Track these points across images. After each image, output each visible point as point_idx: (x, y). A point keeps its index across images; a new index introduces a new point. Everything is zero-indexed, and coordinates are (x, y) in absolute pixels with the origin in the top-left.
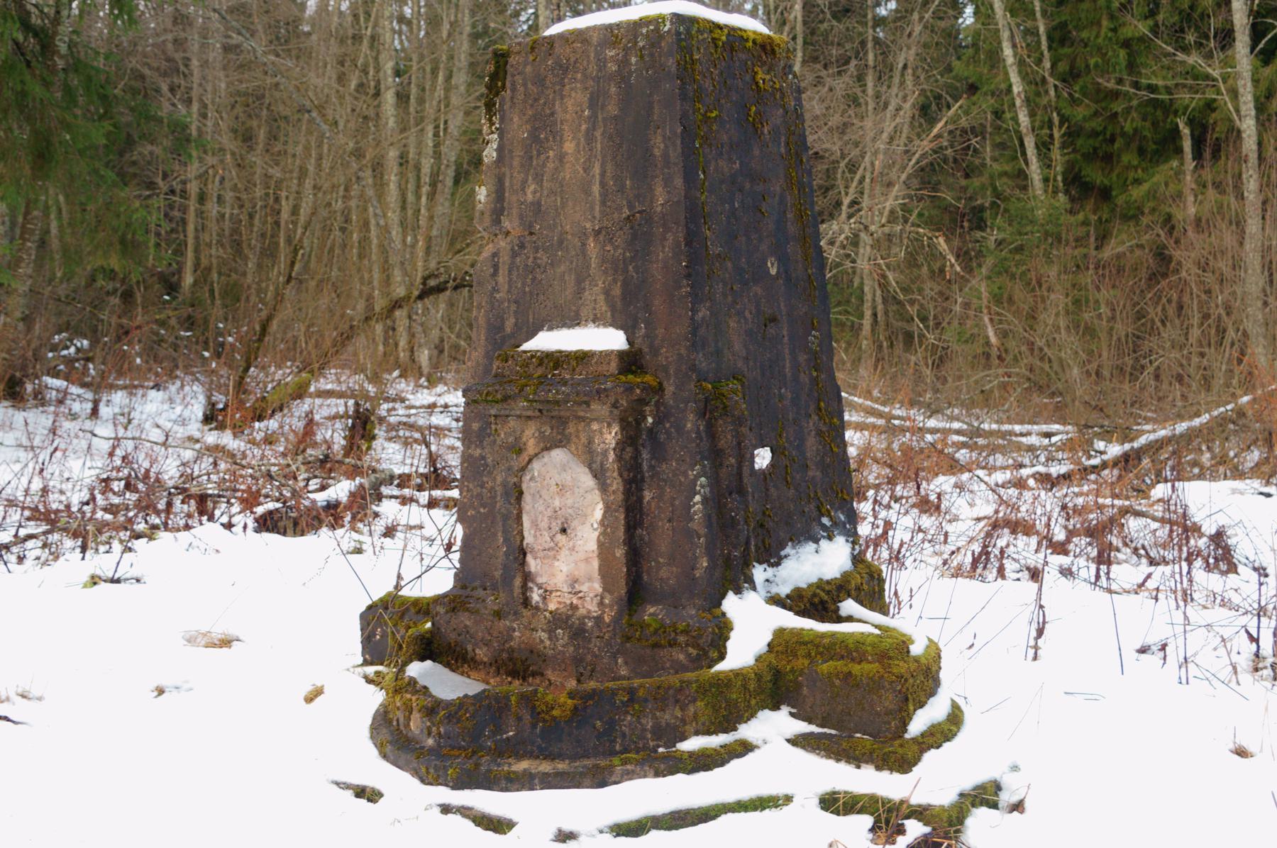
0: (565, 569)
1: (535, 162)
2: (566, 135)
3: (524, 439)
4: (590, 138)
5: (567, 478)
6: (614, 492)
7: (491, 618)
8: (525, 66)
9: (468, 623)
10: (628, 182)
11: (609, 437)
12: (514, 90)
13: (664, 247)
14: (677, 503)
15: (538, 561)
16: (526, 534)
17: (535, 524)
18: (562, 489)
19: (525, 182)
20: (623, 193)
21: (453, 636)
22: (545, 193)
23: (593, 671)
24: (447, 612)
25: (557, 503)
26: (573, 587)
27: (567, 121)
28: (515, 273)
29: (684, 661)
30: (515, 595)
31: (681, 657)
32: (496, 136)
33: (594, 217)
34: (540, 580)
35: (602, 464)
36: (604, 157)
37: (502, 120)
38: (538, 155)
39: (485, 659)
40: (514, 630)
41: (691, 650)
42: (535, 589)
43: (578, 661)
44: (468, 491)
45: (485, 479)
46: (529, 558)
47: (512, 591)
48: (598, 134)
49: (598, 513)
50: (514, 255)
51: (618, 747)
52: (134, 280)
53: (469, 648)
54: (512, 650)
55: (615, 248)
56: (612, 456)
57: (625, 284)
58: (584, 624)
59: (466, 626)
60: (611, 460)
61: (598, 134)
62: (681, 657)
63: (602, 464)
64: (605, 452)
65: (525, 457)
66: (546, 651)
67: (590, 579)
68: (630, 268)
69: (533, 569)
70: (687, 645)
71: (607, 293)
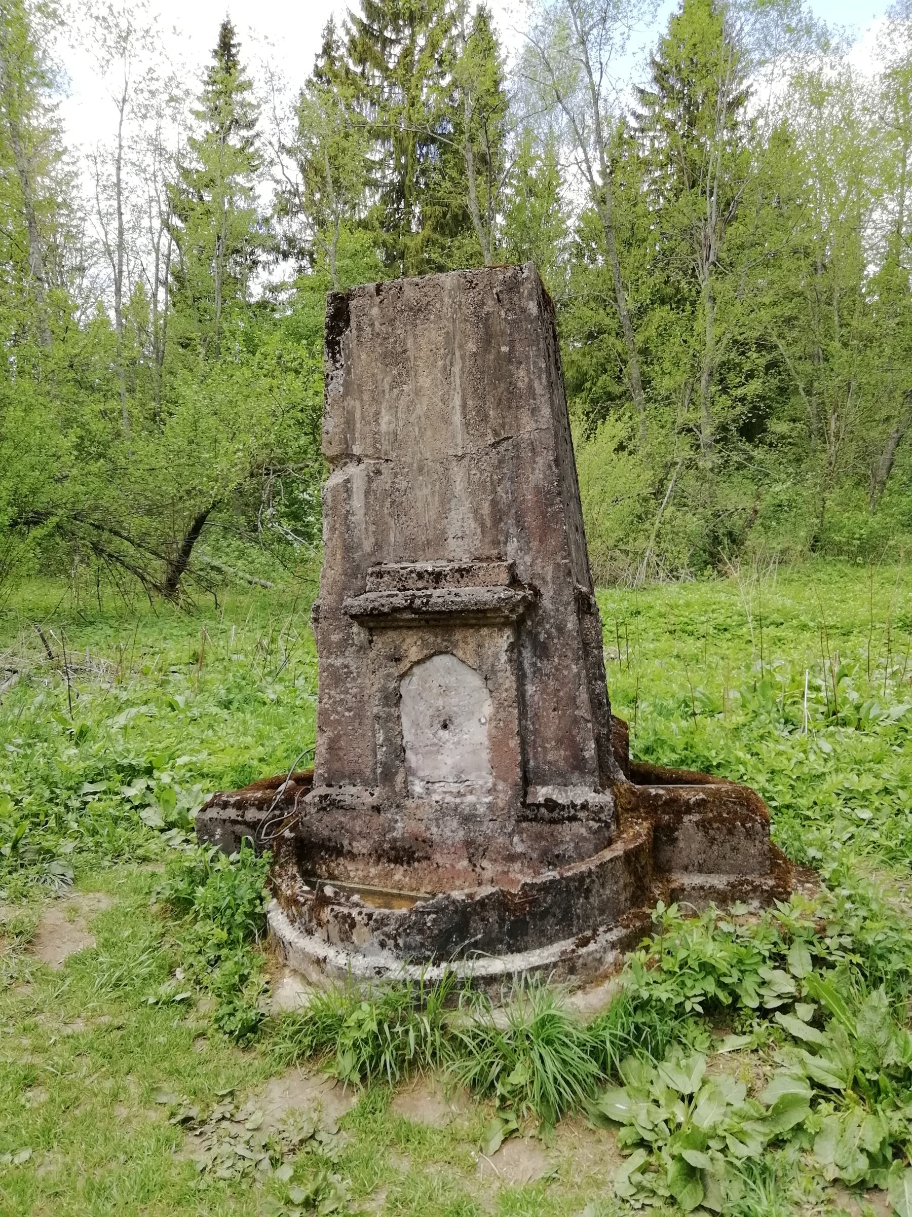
0: (449, 761)
1: (387, 396)
2: (420, 371)
3: (405, 647)
4: (447, 372)
5: (451, 680)
6: (506, 690)
7: (370, 812)
8: (371, 307)
9: (343, 819)
10: (491, 413)
11: (500, 640)
12: (360, 329)
13: (533, 469)
14: (561, 693)
15: (420, 756)
16: (405, 733)
17: (416, 724)
18: (445, 691)
19: (377, 413)
20: (487, 422)
21: (326, 833)
22: (401, 423)
23: (485, 851)
24: (317, 812)
25: (440, 703)
26: (459, 777)
27: (420, 358)
28: (372, 497)
29: (585, 834)
30: (397, 790)
31: (583, 831)
32: (341, 372)
33: (456, 445)
34: (421, 774)
35: (493, 665)
36: (463, 390)
37: (348, 357)
38: (391, 390)
39: (364, 851)
40: (396, 821)
41: (591, 823)
42: (417, 782)
43: (468, 843)
44: (330, 698)
45: (349, 685)
46: (409, 755)
47: (393, 786)
48: (457, 369)
49: (488, 709)
50: (370, 480)
51: (574, 930)
52: (620, 425)
53: (346, 842)
54: (395, 840)
55: (481, 472)
56: (504, 657)
57: (494, 503)
58: (476, 810)
59: (341, 823)
60: (503, 661)
61: (457, 369)
62: (583, 831)
63: (493, 665)
64: (496, 656)
65: (405, 665)
66: (434, 837)
67: (479, 769)
68: (499, 489)
69: (413, 765)
70: (587, 820)
71: (476, 512)
